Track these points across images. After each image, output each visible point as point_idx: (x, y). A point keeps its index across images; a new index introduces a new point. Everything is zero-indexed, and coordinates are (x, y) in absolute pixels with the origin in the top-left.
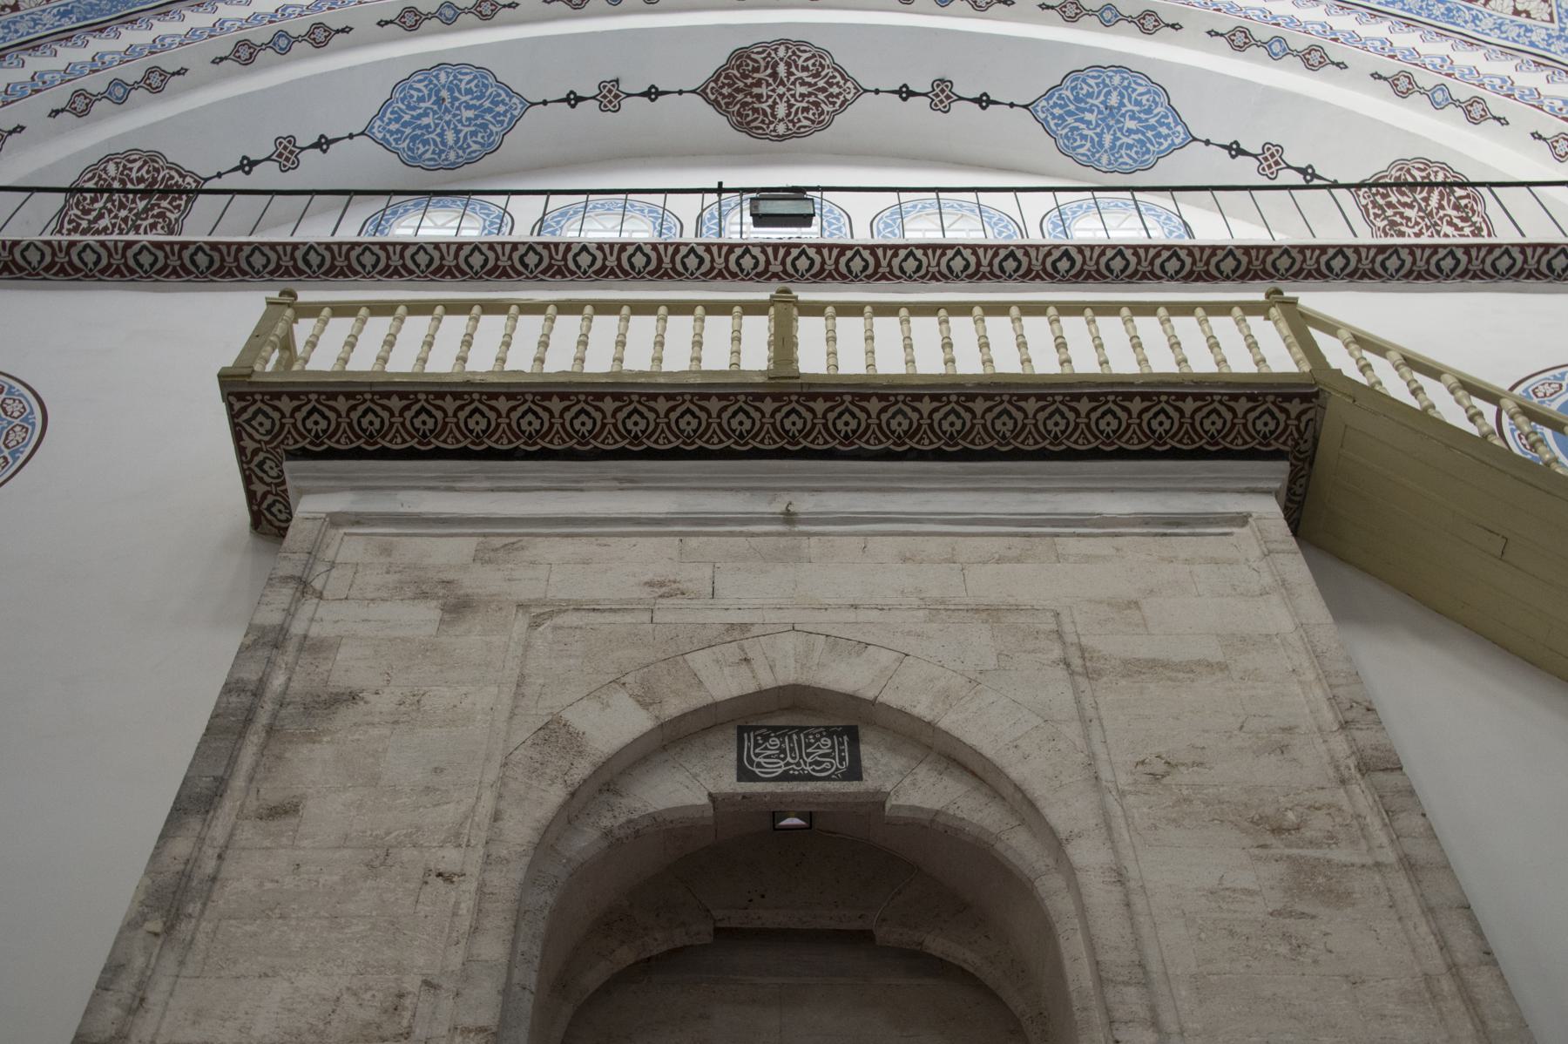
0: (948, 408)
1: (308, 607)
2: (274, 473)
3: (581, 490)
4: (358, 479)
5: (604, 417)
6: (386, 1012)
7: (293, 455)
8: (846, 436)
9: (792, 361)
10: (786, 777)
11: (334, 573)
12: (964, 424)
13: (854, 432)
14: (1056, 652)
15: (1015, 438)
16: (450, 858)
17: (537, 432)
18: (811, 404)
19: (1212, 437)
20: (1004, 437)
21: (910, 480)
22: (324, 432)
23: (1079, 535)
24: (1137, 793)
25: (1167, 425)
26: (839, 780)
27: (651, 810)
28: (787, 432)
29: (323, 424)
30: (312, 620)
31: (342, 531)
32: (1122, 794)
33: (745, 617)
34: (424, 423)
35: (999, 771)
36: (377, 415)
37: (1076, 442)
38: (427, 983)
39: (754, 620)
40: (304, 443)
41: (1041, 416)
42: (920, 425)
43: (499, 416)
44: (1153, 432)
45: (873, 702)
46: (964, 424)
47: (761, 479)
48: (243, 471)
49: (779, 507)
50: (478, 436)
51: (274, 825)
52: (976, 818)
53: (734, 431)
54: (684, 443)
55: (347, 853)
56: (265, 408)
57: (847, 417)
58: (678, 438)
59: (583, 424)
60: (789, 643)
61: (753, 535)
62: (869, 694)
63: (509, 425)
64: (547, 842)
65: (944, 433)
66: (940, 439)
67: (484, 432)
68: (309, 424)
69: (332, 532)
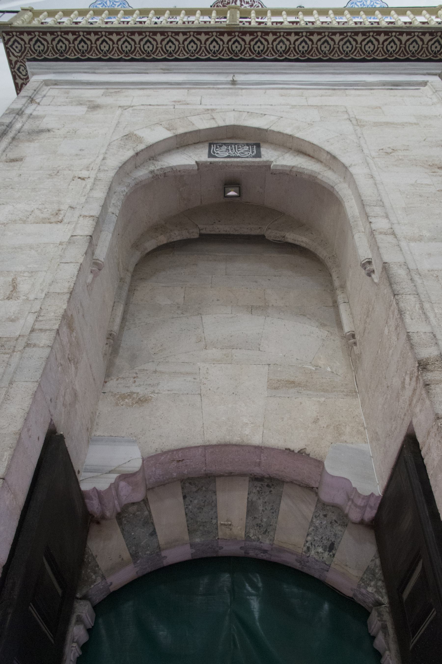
0: (302, 39)
1: (33, 106)
2: (24, 73)
3: (147, 73)
4: (56, 69)
5: (157, 44)
6: (52, 215)
7: (29, 60)
8: (259, 53)
9: (267, 529)
10: (229, 157)
11: (45, 98)
12: (308, 47)
13: (262, 51)
14: (346, 116)
15: (330, 54)
16: (84, 174)
17: (130, 51)
18: (244, 37)
19: (413, 53)
20: (325, 53)
21: (285, 69)
22: (42, 51)
23: (355, 89)
24: (379, 158)
25: (394, 48)
26: (251, 157)
27: (171, 165)
28: (234, 51)
29: (42, 47)
30: (34, 110)
31: (49, 87)
32: (374, 158)
33: (214, 107)
34: (83, 47)
35: (320, 149)
36: (63, 43)
37: (355, 56)
38: (71, 207)
39: (217, 108)
40: (35, 56)
41: (341, 43)
42: (290, 48)
43: (114, 43)
44: (388, 51)
45: (266, 130)
46: (308, 47)
47: (222, 69)
48: (12, 72)
49: (230, 78)
50: (105, 53)
51: (12, 164)
52: (310, 168)
53: (211, 51)
54: (191, 56)
55: (41, 172)
56: (18, 39)
57: (259, 44)
58: (188, 53)
59: (148, 47)
60: (232, 114)
61: (218, 89)
62: (266, 127)
63: (118, 48)
64: (123, 170)
65: (300, 51)
66: (298, 54)
67: (108, 51)
68: (36, 47)
69: (45, 87)
